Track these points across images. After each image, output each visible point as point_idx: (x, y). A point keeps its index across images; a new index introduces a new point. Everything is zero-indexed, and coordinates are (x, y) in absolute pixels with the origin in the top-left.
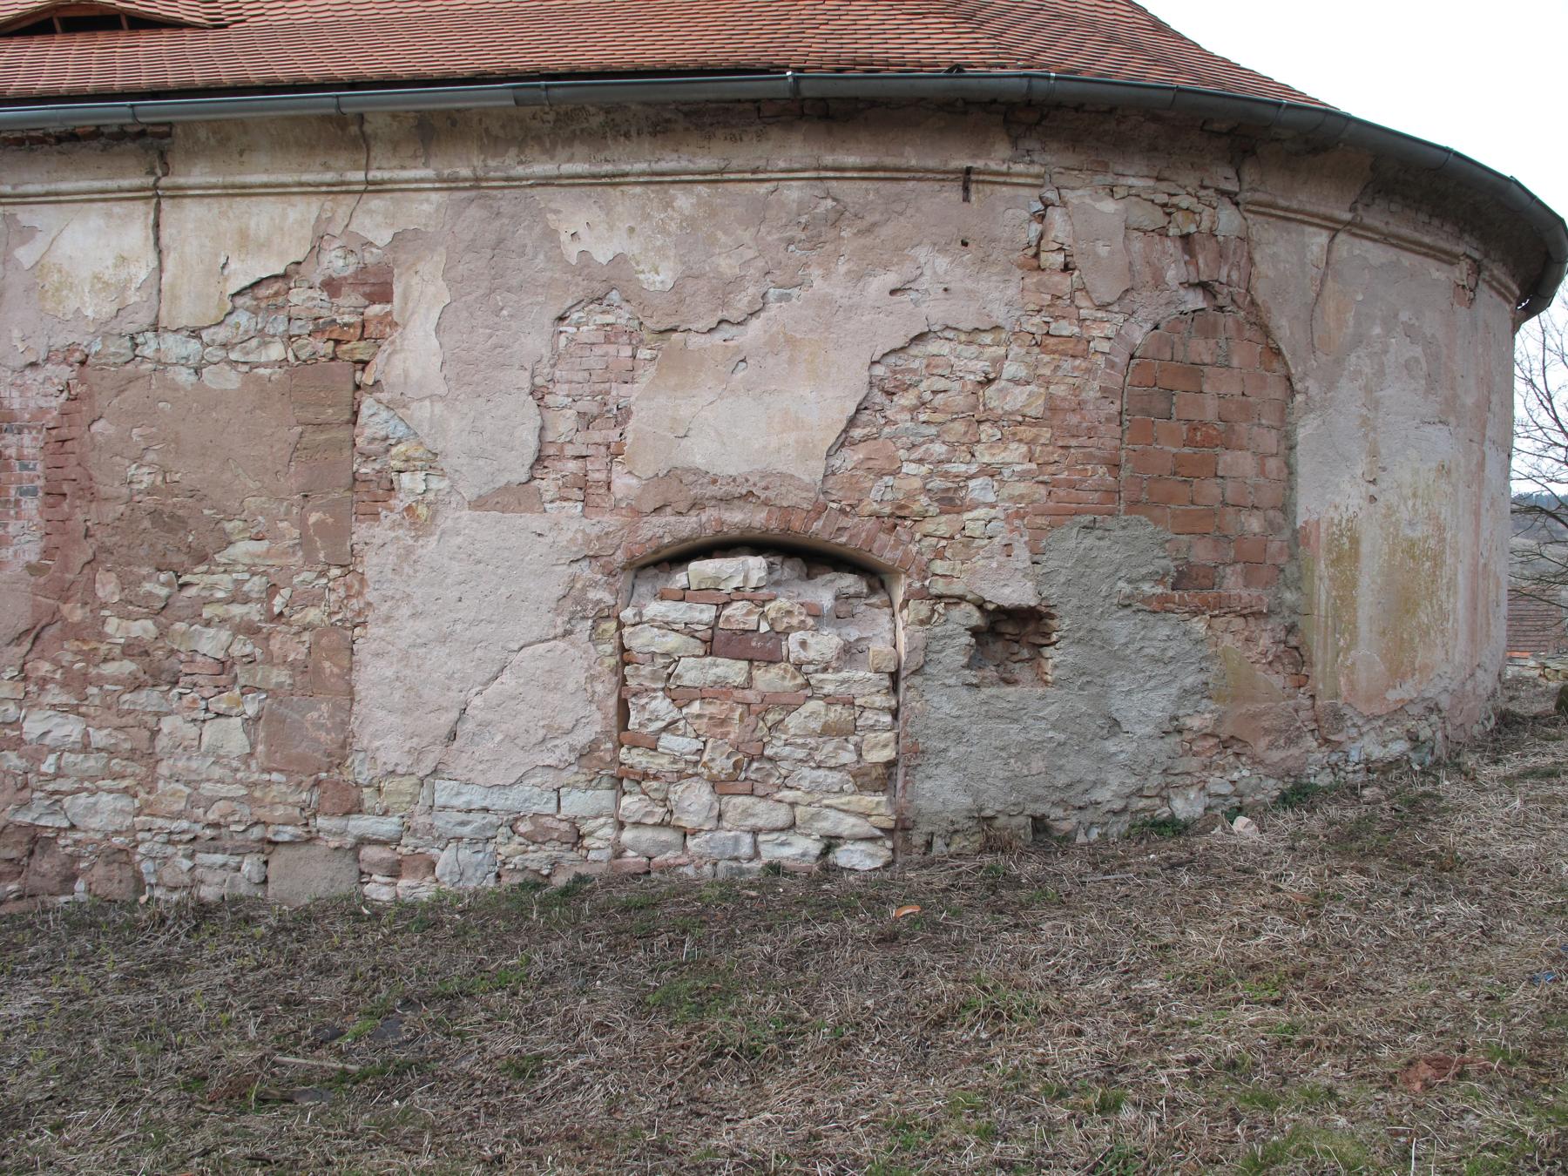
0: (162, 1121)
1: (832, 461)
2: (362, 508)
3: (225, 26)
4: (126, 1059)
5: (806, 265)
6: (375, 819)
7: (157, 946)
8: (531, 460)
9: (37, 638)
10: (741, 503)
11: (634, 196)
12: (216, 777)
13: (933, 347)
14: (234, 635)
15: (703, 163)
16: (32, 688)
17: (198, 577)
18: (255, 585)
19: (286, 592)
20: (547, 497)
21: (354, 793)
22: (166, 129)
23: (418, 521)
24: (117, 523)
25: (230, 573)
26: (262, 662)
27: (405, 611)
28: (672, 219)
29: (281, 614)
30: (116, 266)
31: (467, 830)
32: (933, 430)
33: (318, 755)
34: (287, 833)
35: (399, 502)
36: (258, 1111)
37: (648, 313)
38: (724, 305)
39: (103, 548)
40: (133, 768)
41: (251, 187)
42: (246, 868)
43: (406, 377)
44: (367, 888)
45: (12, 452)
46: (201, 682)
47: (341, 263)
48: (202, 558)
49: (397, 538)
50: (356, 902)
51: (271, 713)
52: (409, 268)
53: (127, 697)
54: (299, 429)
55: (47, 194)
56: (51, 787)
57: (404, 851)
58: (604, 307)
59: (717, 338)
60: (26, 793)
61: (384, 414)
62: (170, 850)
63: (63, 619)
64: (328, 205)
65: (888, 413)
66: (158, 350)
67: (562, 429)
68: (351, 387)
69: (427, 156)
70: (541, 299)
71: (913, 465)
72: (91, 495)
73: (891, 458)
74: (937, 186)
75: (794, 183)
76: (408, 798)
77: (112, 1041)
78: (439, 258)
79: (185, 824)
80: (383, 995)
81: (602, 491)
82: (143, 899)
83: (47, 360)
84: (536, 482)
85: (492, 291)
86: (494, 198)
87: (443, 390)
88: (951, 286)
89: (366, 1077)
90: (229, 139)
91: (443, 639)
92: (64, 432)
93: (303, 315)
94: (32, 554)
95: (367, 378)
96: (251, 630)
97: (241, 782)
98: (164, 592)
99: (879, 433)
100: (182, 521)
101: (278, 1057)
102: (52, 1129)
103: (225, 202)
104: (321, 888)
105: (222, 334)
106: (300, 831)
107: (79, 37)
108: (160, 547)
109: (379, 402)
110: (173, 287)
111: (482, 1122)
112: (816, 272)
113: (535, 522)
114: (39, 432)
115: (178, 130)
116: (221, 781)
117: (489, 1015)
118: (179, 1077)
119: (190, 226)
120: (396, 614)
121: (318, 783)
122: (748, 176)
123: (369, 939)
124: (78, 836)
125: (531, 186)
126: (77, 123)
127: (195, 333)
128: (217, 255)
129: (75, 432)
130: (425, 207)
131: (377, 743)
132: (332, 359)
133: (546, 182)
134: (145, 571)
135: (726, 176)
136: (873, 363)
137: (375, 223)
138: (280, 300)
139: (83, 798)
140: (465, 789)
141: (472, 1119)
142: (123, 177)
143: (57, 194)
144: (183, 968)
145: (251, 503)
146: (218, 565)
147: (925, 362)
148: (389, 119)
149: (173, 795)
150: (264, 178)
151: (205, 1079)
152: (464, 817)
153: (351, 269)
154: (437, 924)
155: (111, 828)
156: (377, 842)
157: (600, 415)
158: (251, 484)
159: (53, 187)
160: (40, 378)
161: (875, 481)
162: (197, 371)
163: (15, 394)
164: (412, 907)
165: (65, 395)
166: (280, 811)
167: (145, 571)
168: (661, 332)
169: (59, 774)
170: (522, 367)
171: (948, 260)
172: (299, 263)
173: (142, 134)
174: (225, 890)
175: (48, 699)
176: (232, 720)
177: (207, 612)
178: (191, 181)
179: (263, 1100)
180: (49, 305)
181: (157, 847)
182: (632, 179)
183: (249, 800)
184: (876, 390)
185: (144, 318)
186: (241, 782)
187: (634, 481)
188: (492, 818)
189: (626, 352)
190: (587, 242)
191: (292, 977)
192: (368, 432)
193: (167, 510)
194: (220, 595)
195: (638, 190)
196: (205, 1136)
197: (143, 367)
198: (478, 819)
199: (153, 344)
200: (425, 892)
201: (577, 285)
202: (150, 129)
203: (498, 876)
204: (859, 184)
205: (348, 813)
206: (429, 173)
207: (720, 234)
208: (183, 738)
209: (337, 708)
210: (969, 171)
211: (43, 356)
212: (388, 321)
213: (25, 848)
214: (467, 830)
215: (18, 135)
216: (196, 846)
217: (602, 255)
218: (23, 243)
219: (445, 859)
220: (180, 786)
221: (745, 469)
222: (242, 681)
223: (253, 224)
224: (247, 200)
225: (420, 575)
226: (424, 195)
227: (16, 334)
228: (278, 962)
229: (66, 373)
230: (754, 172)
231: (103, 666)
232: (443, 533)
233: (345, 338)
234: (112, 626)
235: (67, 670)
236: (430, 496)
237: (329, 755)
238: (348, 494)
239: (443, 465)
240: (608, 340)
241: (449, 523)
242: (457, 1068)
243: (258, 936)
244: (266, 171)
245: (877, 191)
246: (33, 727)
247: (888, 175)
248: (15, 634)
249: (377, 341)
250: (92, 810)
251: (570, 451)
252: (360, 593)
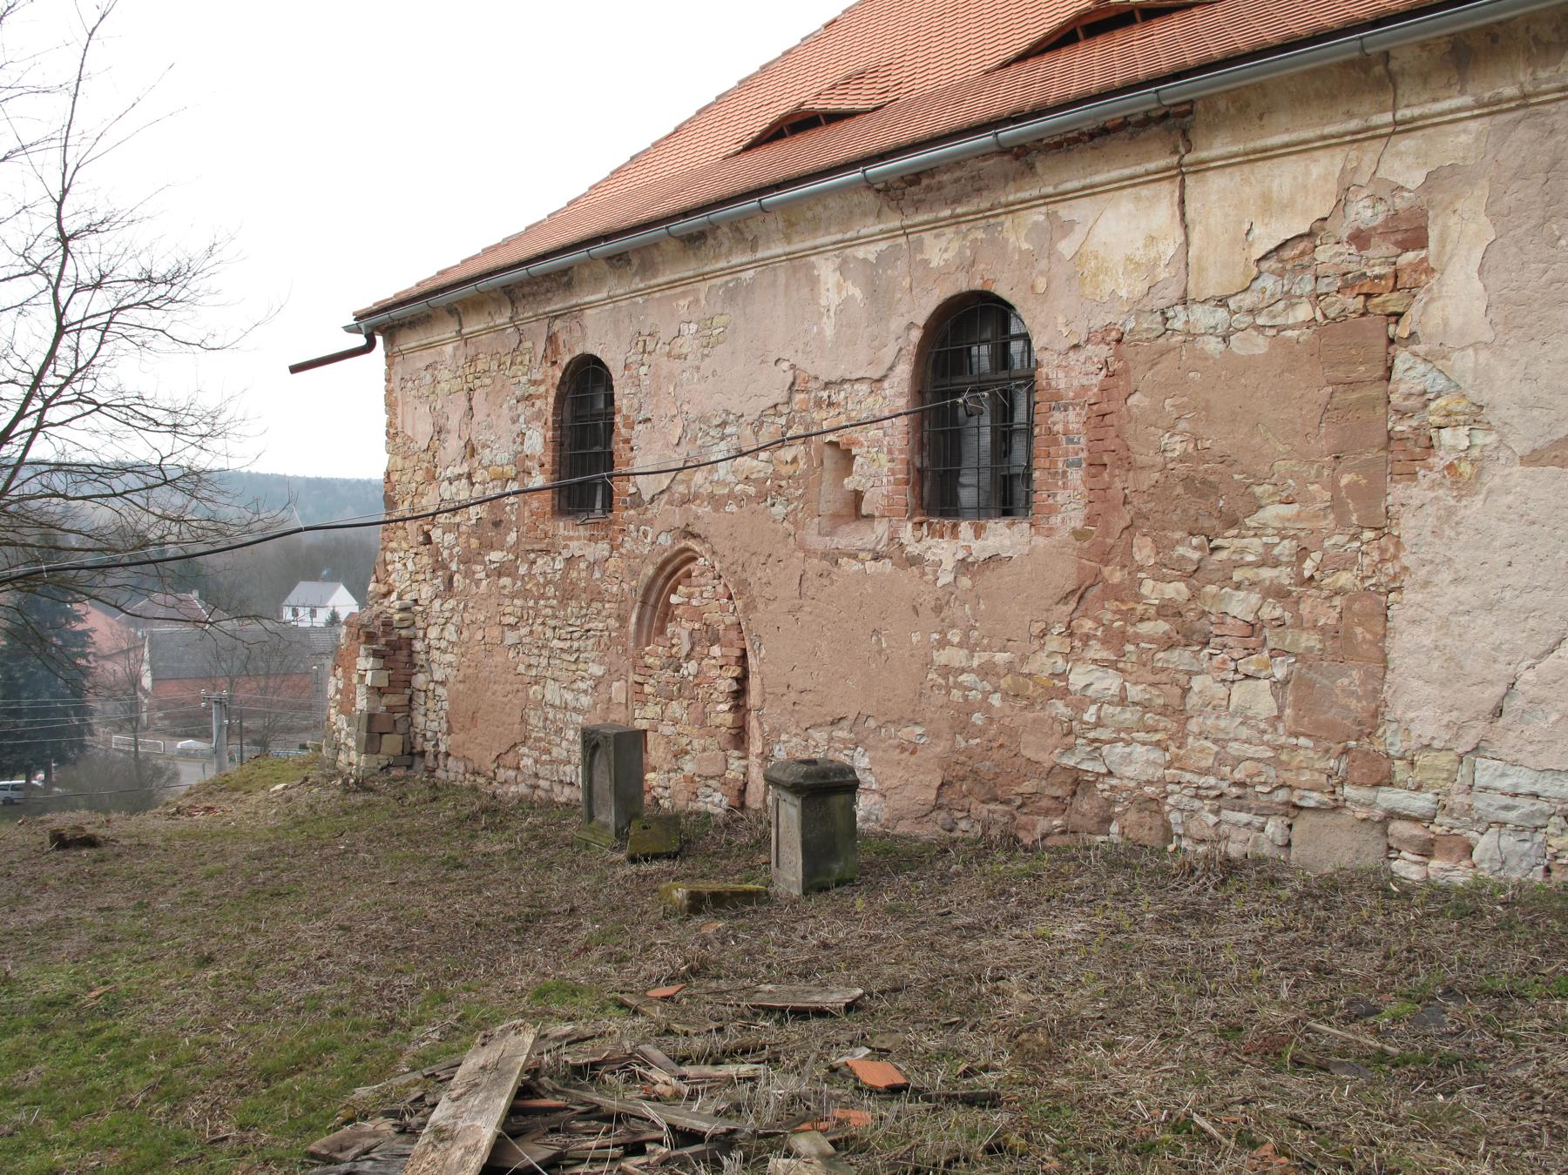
0: (1200, 1061)
2: (1398, 468)
4: (1165, 996)
6: (1406, 793)
7: (1187, 894)
9: (1081, 597)
12: (1244, 737)
14: (1264, 599)
16: (1077, 643)
17: (1230, 542)
18: (1285, 549)
19: (1317, 556)
21: (1386, 764)
22: (1187, 107)
23: (1460, 479)
25: (1260, 537)
26: (1291, 626)
27: (1446, 575)
29: (1312, 578)
30: (1146, 246)
31: (1511, 816)
33: (1348, 722)
34: (1313, 799)
35: (1439, 460)
36: (1293, 1072)
39: (1140, 514)
40: (1164, 722)
41: (1272, 149)
42: (1269, 829)
43: (1445, 325)
44: (1395, 865)
45: (1059, 428)
46: (1231, 644)
47: (1369, 212)
48: (1233, 522)
49: (1437, 498)
50: (1384, 877)
51: (1300, 677)
52: (1446, 208)
53: (1160, 655)
54: (1330, 389)
55: (1084, 188)
56: (1091, 735)
57: (1438, 830)
60: (1071, 739)
61: (1421, 368)
62: (1197, 804)
63: (1104, 581)
64: (1353, 154)
66: (1187, 322)
68: (1384, 341)
69: (1463, 81)
72: (1129, 465)
76: (1445, 775)
77: (1152, 977)
78: (1482, 192)
79: (1212, 781)
80: (1422, 979)
82: (1171, 848)
83: (1088, 341)
85: (1546, 220)
86: (1547, 114)
87: (1488, 336)
89: (1406, 1062)
90: (1248, 105)
91: (1489, 607)
92: (1104, 407)
93: (1331, 272)
94: (1077, 523)
95: (1402, 331)
96: (1280, 594)
97: (1267, 744)
98: (1196, 555)
100: (1213, 487)
101: (1312, 1023)
102: (1104, 1045)
103: (1246, 168)
104: (1345, 858)
105: (1248, 300)
106: (1326, 798)
107: (1099, 40)
108: (1192, 512)
109: (1415, 355)
110: (1199, 259)
111: (1546, 1144)
114: (1082, 408)
115: (1199, 106)
116: (1248, 741)
117: (1547, 1024)
118: (1216, 1024)
119: (1214, 197)
120: (1435, 579)
121: (1346, 751)
123: (1399, 918)
124: (1114, 782)
126: (1107, 118)
127: (1222, 302)
128: (1241, 222)
129: (1113, 406)
130: (1463, 138)
131: (1411, 715)
132: (1363, 315)
134: (1178, 535)
137: (1405, 165)
139: (1119, 748)
140: (1511, 771)
141: (1532, 1135)
142: (1150, 160)
143: (1092, 187)
144: (1212, 920)
145: (1281, 466)
146: (1248, 529)
148: (1417, 51)
149: (1201, 751)
150: (1286, 138)
151: (1240, 1029)
152: (1508, 801)
153: (1381, 218)
154: (1476, 913)
155: (1144, 778)
156: (1408, 818)
158: (1281, 448)
159: (1088, 181)
160: (1082, 359)
162: (1225, 339)
164: (1446, 890)
165: (1104, 372)
166: (1306, 777)
167: (1178, 535)
169: (1098, 724)
173: (1166, 116)
174: (1248, 849)
175: (1091, 654)
176: (1261, 682)
177: (1237, 575)
178: (1213, 153)
179: (1298, 1063)
180: (1088, 290)
181: (1185, 800)
183: (1275, 762)
185: (1173, 293)
186: (1267, 744)
188: (1541, 805)
191: (1321, 944)
192: (1403, 388)
193: (1198, 476)
194: (1250, 558)
196: (1241, 1086)
198: (1526, 806)
199: (1182, 317)
200: (1460, 876)
202: (1172, 110)
203: (1548, 870)
205: (1377, 785)
206: (1467, 100)
208: (1213, 697)
209: (1370, 675)
211: (1084, 338)
213: (1068, 788)
214: (1511, 816)
215: (1057, 139)
216: (1221, 802)
219: (1485, 844)
220: (1208, 744)
222: (1271, 644)
223: (1275, 187)
224: (1268, 163)
225: (1464, 538)
226: (1461, 126)
227: (1061, 319)
228: (1306, 928)
229: (1104, 351)
231: (1139, 625)
232: (1490, 492)
233: (1377, 290)
234: (1147, 587)
235: (1108, 628)
236: (1475, 453)
237: (1360, 723)
238: (1383, 453)
239: (1490, 418)
242: (1512, 1075)
243: (1284, 898)
244: (1287, 130)
246: (1077, 679)
248: (1062, 594)
249: (1412, 291)
250: (1127, 759)
252: (1395, 557)
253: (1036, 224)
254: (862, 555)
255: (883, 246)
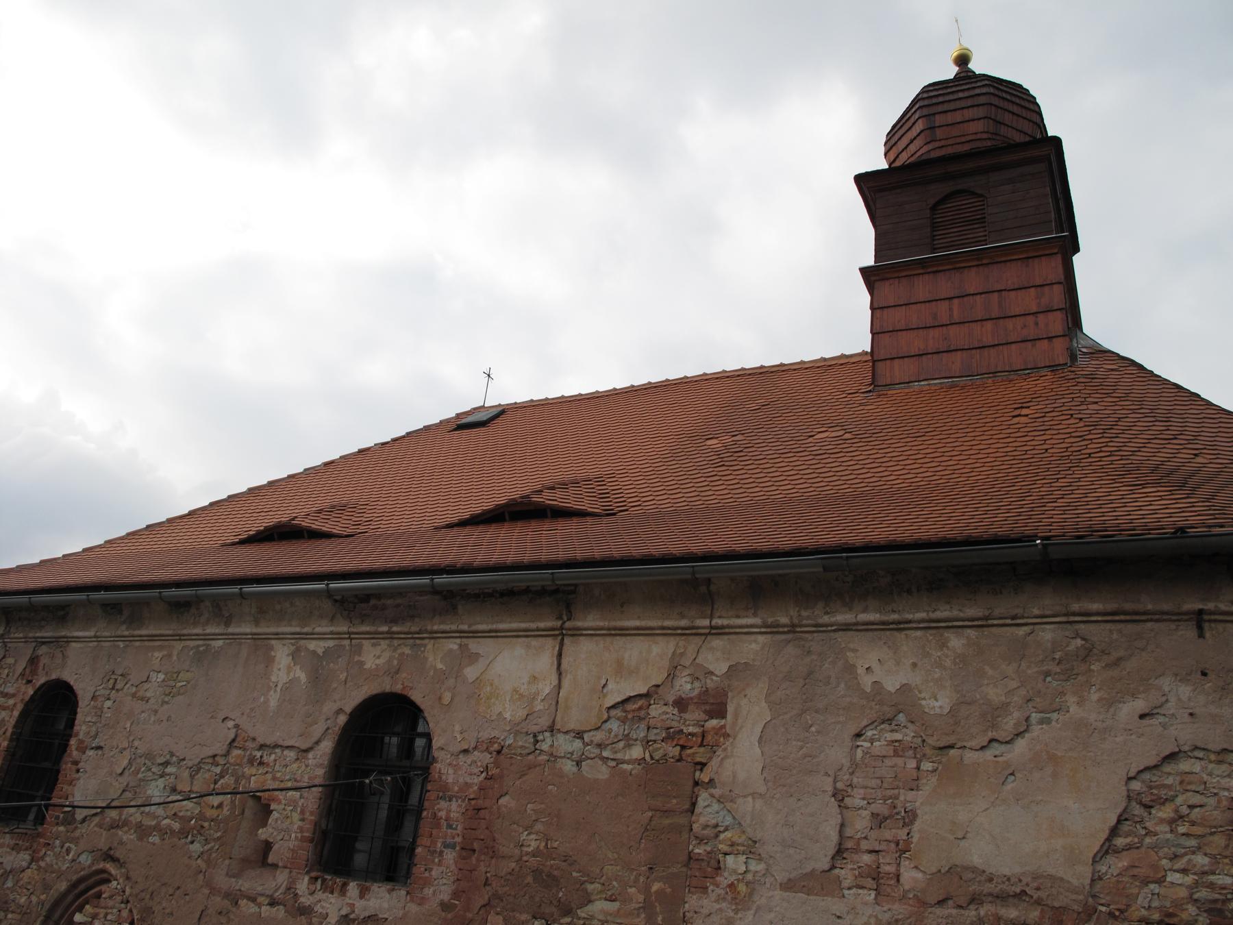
1: (1098, 868)
3: (614, 514)
5: (1062, 694)
8: (831, 852)
10: (1016, 901)
11: (916, 638)
13: (1184, 766)
15: (971, 612)
20: (846, 883)
23: (740, 897)
24: (508, 877)
28: (947, 656)
32: (1193, 842)
35: (725, 879)
37: (930, 732)
38: (994, 726)
39: (496, 896)
45: (442, 814)
47: (689, 686)
49: (721, 910)
54: (650, 814)
55: (490, 631)
58: (893, 727)
59: (989, 754)
61: (716, 806)
64: (681, 643)
65: (1147, 824)
66: (552, 746)
67: (858, 827)
68: (691, 783)
70: (842, 719)
71: (1178, 875)
72: (493, 853)
73: (1155, 867)
74: (1173, 626)
75: (1048, 627)
81: (892, 882)
83: (475, 748)
84: (837, 871)
85: (804, 711)
87: (763, 789)
88: (1196, 711)
99: (1141, 842)
103: (608, 639)
105: (598, 736)
107: (519, 524)
108: (537, 899)
109: (712, 796)
112: (1071, 700)
113: (837, 906)
114: (463, 801)
122: (1009, 621)
125: (834, 631)
127: (579, 735)
128: (599, 678)
130: (753, 646)
132: (678, 761)
133: (846, 627)
135: (990, 622)
136: (1130, 779)
137: (715, 659)
138: (642, 713)
143: (496, 631)
146: (579, 918)
147: (1178, 778)
150: (637, 623)
153: (696, 692)
157: (890, 817)
160: (469, 762)
161: (1141, 888)
162: (578, 763)
163: (451, 771)
165: (484, 775)
168: (940, 748)
170: (827, 774)
171: (1189, 688)
172: (658, 686)
173: (556, 591)
182: (914, 625)
184: (1134, 804)
185: (544, 722)
187: (920, 875)
189: (912, 764)
190: (879, 674)
192: (702, 820)
195: (919, 633)
197: (540, 758)
201: (871, 708)
204: (1103, 626)
206: (757, 621)
207: (987, 668)
210: (1201, 612)
211: (473, 745)
212: (721, 732)
217: (891, 685)
218: (470, 664)
221: (1017, 870)
223: (627, 656)
224: (624, 639)
226: (753, 637)
227: (457, 728)
229: (487, 758)
230: (1013, 618)
232: (759, 908)
236: (749, 877)
238: (684, 869)
239: (761, 851)
240: (896, 754)
241: (763, 901)
244: (639, 618)
245: (1120, 631)
247: (1128, 618)
249: (713, 749)
251: (865, 845)
253: (451, 651)
254: (260, 899)
255: (331, 643)
